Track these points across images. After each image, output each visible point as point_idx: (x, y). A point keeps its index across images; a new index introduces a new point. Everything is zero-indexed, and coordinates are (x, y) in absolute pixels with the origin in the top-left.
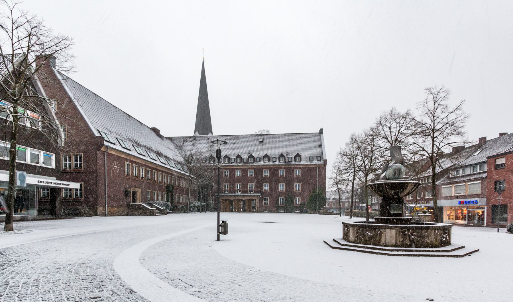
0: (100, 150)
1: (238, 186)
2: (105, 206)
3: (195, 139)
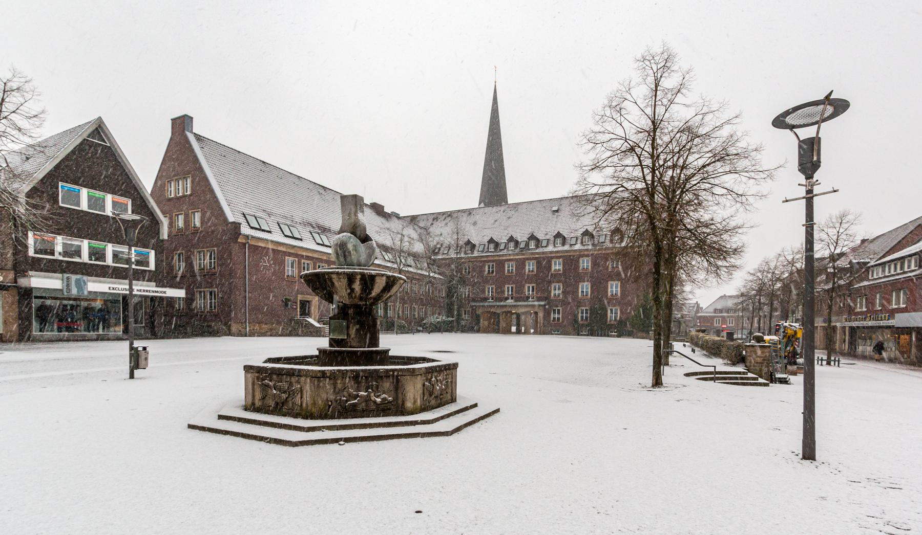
0: (236, 242)
1: (508, 289)
2: (246, 322)
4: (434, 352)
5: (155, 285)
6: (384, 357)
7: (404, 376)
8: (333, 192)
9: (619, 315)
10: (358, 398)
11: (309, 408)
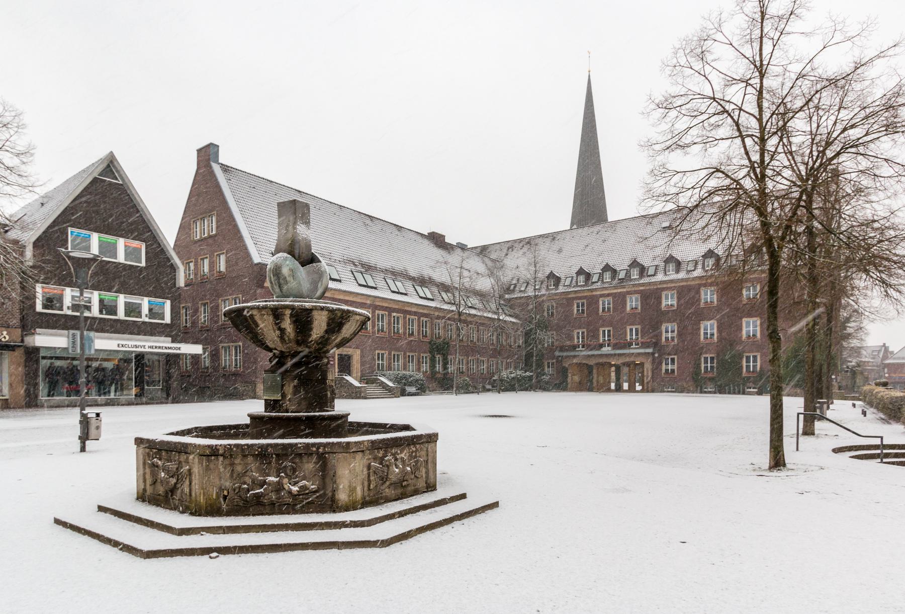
3: (529, 243)
4: (486, 416)
5: (170, 341)
6: (341, 425)
7: (335, 453)
8: (382, 222)
9: (759, 364)
10: (265, 486)
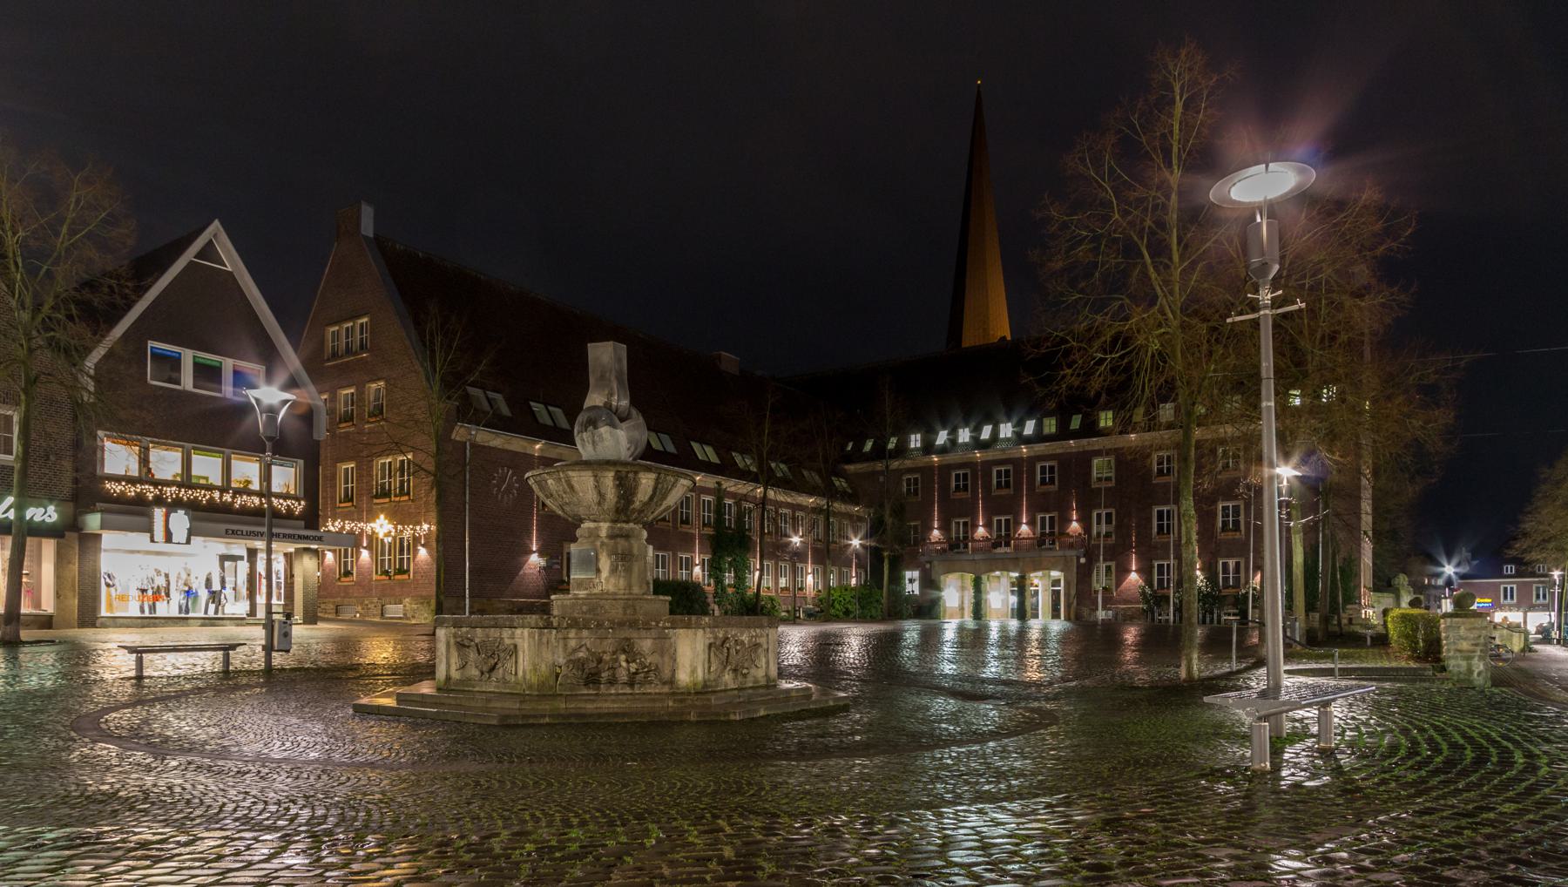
11: (528, 677)
